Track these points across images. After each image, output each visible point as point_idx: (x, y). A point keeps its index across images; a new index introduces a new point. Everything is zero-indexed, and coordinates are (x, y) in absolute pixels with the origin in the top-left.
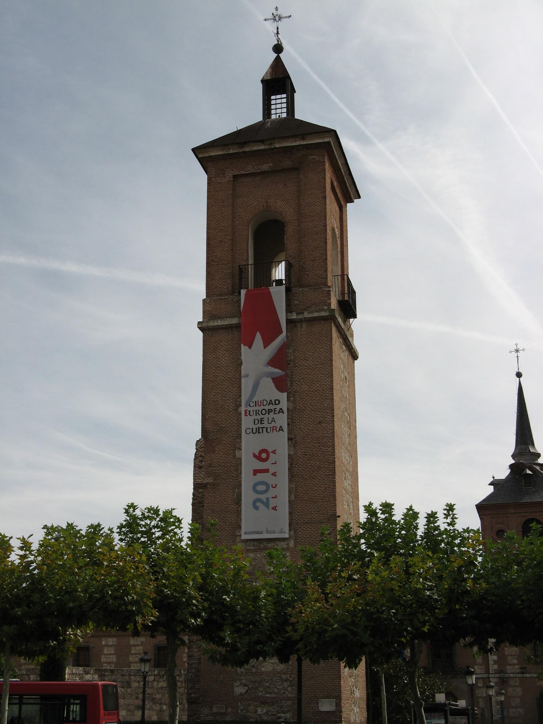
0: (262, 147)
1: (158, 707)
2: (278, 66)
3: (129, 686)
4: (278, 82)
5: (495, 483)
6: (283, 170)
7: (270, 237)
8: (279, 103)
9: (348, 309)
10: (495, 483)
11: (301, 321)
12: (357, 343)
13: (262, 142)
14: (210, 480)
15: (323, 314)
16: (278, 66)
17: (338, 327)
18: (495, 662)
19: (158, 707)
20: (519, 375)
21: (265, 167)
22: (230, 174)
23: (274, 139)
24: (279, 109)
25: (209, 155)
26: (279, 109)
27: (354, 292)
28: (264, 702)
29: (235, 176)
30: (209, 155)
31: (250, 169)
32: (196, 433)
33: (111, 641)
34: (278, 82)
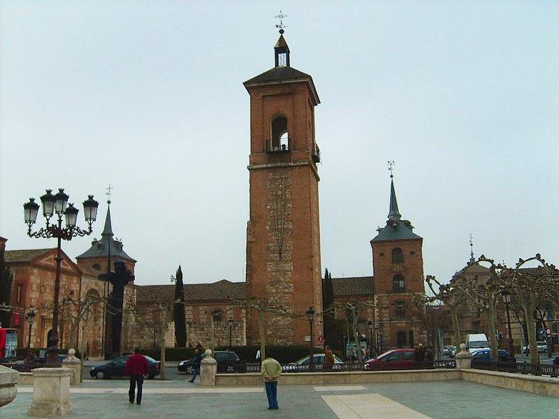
0: (276, 83)
1: (217, 340)
2: (282, 40)
3: (203, 329)
4: (282, 48)
5: (379, 230)
6: (286, 94)
7: (280, 125)
8: (282, 57)
9: (316, 159)
10: (379, 230)
11: (296, 166)
12: (319, 173)
13: (276, 80)
14: (254, 240)
15: (306, 163)
16: (282, 40)
17: (312, 168)
18: (377, 312)
19: (217, 340)
20: (392, 176)
21: (278, 92)
22: (261, 95)
23: (313, 144)
24: (282, 63)
25: (251, 86)
26: (282, 63)
27: (318, 151)
28: (281, 338)
29: (263, 96)
30: (251, 86)
31: (271, 93)
32: (246, 218)
33: (190, 308)
34: (282, 48)
